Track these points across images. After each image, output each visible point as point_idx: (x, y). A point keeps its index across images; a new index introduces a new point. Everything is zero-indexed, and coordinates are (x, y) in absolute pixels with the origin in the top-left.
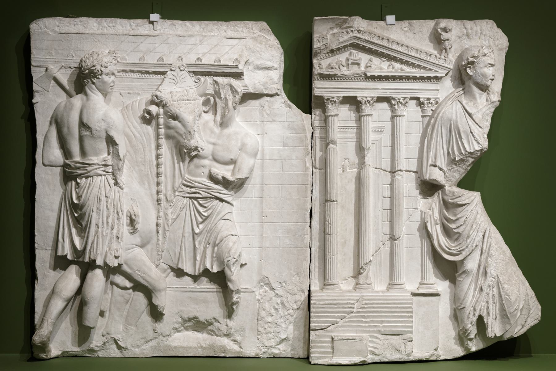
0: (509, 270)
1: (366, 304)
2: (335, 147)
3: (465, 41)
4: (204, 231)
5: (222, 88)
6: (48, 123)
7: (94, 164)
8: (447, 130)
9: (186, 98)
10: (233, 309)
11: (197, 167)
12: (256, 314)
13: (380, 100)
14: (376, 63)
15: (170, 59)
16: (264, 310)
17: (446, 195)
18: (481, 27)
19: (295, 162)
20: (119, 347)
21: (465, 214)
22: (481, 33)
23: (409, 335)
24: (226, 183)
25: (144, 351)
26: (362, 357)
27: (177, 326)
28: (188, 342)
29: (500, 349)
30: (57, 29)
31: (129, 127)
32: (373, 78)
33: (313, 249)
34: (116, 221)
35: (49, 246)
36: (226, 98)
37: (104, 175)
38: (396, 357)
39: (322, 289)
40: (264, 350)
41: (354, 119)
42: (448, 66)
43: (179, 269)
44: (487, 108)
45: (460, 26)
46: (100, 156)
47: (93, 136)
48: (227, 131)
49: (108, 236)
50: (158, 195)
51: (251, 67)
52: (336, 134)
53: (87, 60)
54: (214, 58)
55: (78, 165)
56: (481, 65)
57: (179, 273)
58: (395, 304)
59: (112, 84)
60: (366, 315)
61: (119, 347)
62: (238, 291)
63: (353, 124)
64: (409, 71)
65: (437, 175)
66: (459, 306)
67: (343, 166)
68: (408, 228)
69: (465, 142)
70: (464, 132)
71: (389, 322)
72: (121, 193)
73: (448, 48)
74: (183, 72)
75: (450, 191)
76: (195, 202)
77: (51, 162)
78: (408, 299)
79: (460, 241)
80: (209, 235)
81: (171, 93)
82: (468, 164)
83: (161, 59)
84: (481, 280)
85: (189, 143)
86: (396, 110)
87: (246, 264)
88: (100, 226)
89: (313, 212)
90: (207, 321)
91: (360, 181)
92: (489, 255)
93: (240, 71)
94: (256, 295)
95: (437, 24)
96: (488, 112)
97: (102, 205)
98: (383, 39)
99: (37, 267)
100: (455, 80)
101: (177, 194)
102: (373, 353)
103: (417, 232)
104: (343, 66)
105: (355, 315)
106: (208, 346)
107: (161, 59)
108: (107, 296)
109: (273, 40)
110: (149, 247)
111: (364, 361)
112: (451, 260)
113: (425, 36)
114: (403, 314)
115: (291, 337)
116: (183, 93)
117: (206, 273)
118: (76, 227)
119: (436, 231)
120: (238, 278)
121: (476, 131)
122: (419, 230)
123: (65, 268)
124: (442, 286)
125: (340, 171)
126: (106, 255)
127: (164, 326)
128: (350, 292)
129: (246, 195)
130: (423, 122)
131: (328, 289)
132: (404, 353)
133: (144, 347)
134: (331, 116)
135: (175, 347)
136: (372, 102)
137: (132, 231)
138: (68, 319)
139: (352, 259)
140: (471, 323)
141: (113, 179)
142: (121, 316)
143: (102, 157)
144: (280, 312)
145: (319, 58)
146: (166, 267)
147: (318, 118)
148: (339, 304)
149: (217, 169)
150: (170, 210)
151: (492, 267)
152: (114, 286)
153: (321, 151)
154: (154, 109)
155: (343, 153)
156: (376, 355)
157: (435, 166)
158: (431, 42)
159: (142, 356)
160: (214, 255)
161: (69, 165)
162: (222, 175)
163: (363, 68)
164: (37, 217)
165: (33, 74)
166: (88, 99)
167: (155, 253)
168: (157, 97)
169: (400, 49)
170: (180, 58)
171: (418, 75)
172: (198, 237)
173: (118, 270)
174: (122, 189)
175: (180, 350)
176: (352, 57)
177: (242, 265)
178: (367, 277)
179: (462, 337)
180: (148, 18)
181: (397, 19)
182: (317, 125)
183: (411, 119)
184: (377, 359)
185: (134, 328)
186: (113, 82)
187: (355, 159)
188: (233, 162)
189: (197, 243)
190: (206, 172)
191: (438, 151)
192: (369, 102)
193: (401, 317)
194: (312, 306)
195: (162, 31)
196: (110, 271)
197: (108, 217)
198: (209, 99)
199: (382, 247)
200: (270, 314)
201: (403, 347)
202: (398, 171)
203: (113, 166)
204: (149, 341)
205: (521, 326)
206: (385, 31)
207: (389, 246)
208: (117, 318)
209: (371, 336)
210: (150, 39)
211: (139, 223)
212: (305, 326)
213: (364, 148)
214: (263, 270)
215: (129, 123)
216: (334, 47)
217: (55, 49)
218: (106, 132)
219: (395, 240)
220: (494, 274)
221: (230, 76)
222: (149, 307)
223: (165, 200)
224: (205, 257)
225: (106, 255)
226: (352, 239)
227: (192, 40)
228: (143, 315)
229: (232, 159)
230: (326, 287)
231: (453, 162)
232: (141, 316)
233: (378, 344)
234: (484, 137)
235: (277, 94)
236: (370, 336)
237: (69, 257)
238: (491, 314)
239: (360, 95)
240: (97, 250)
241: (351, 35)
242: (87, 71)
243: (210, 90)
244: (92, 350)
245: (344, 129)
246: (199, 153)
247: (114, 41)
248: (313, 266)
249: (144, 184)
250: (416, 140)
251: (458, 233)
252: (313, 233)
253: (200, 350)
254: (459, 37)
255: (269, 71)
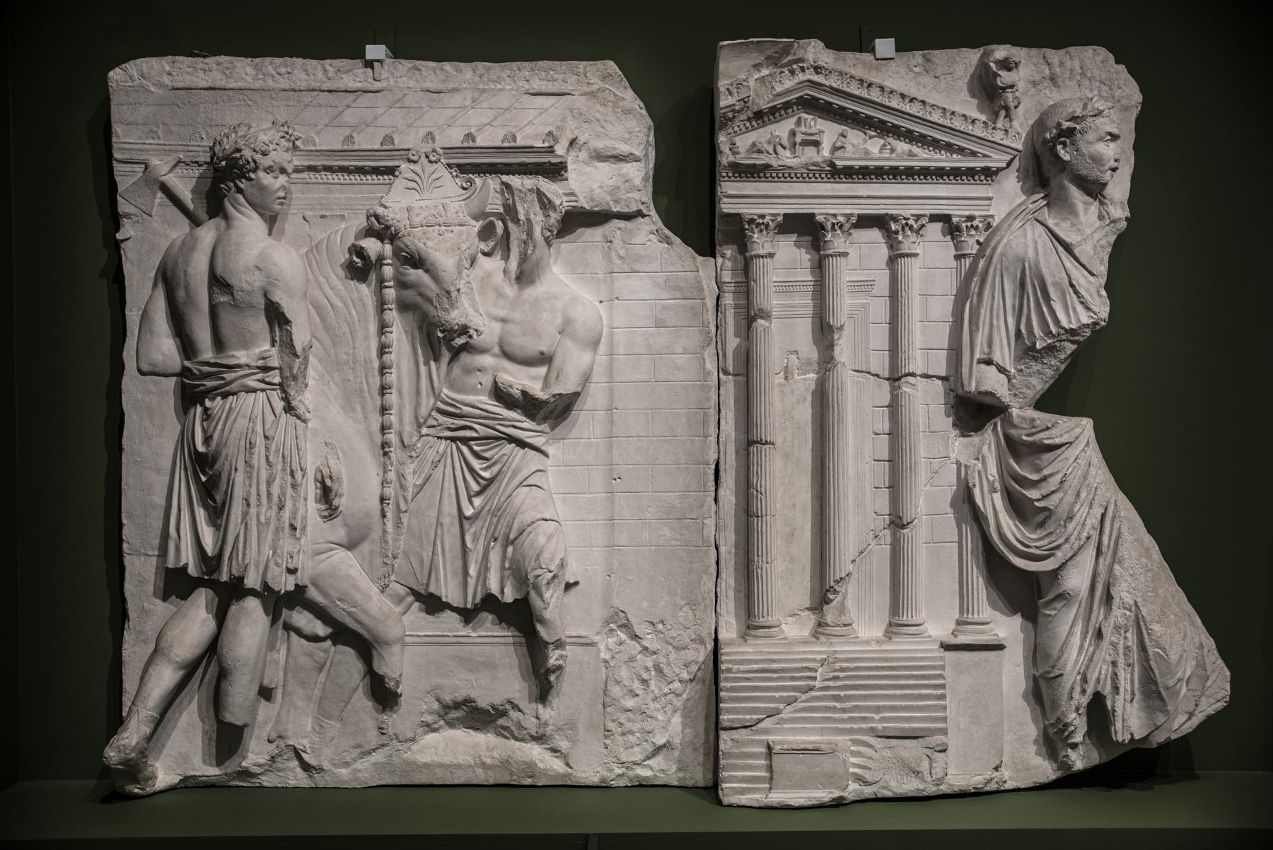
0: (1160, 592)
1: (842, 670)
2: (767, 324)
3: (1047, 91)
4: (484, 513)
5: (521, 198)
6: (150, 284)
7: (239, 366)
8: (1014, 282)
9: (441, 220)
10: (549, 682)
11: (468, 371)
12: (601, 693)
13: (865, 222)
14: (855, 142)
15: (410, 139)
16: (618, 682)
17: (1015, 426)
18: (1082, 61)
19: (681, 360)
20: (306, 767)
21: (1056, 466)
22: (1083, 74)
23: (939, 739)
24: (529, 405)
25: (359, 775)
26: (837, 788)
27: (429, 718)
28: (454, 752)
29: (1132, 767)
30: (166, 80)
31: (321, 288)
32: (850, 173)
33: (722, 549)
34: (289, 491)
35: (152, 549)
36: (529, 220)
37: (263, 390)
38: (910, 786)
39: (744, 636)
40: (618, 771)
41: (809, 264)
42: (1013, 145)
43: (431, 595)
44: (1103, 233)
45: (1035, 60)
46: (256, 348)
47: (235, 305)
48: (530, 292)
49: (272, 526)
50: (384, 434)
51: (583, 155)
52: (769, 296)
53: (225, 140)
54: (502, 133)
55: (207, 369)
56: (1091, 136)
57: (433, 604)
58: (906, 668)
59: (282, 194)
60: (842, 694)
61: (306, 767)
62: (559, 644)
63: (806, 275)
64: (925, 157)
65: (993, 382)
66: (1049, 672)
67: (786, 367)
68: (930, 499)
69: (1057, 306)
70: (1056, 284)
71: (893, 709)
72: (300, 432)
73: (1012, 105)
74: (435, 166)
75: (1024, 418)
76: (465, 449)
77: (153, 365)
78: (936, 658)
79: (1051, 526)
80: (495, 520)
81: (409, 209)
82: (1062, 357)
83: (388, 139)
84: (1098, 614)
85: (448, 318)
86: (900, 242)
87: (576, 583)
88: (253, 501)
89: (722, 468)
90: (493, 707)
91: (823, 400)
92: (1115, 559)
93: (558, 160)
94: (599, 651)
95: (986, 55)
96: (1103, 242)
97: (255, 456)
98: (870, 85)
99: (127, 594)
100: (1027, 177)
101: (425, 430)
102: (858, 778)
103: (950, 510)
104: (784, 148)
105: (818, 693)
106: (496, 762)
107: (388, 139)
108: (275, 655)
109: (629, 97)
110: (365, 548)
111: (842, 798)
112: (1030, 569)
113: (960, 83)
114: (924, 692)
115: (677, 741)
116: (434, 209)
117: (490, 603)
118: (205, 506)
119: (993, 505)
120: (561, 615)
121: (1082, 281)
122: (954, 504)
123: (184, 597)
124: (1007, 628)
125: (779, 379)
126: (266, 567)
127: (399, 721)
128: (805, 643)
129: (575, 432)
130: (959, 269)
131: (757, 636)
132: (929, 778)
133: (359, 765)
134: (759, 256)
135: (426, 765)
136: (847, 226)
137: (326, 513)
138: (194, 706)
139: (808, 570)
140: (1077, 710)
141: (283, 399)
142: (309, 698)
143: (257, 351)
144: (653, 687)
145: (730, 130)
146: (402, 591)
147: (729, 264)
148: (783, 670)
149: (510, 374)
150: (410, 468)
151: (1124, 584)
152: (292, 633)
153: (736, 335)
154: (372, 246)
155: (785, 338)
156: (866, 783)
157: (989, 362)
158: (973, 95)
159: (354, 785)
160: (507, 565)
161: (189, 370)
162: (520, 387)
163: (826, 153)
164: (127, 485)
165: (118, 179)
166: (228, 226)
167: (378, 561)
168: (377, 217)
169: (907, 108)
170: (430, 136)
171: (947, 165)
172: (471, 524)
173: (297, 598)
174: (304, 421)
175: (437, 771)
176: (803, 129)
177: (569, 586)
178: (842, 609)
179: (1053, 740)
180: (360, 55)
181: (899, 49)
182: (728, 280)
183: (932, 265)
184: (868, 791)
185: (338, 725)
186: (284, 188)
187: (809, 351)
188: (544, 359)
189: (468, 538)
190: (487, 381)
191: (995, 330)
192: (841, 227)
193: (921, 697)
194: (722, 676)
195: (392, 81)
196: (278, 603)
197: (269, 483)
198: (492, 224)
199: (873, 543)
200: (631, 691)
201: (925, 764)
202: (907, 375)
203: (281, 369)
204: (369, 753)
205: (1186, 716)
206: (874, 73)
207: (889, 540)
208: (300, 703)
209: (855, 742)
210: (365, 100)
211: (341, 496)
212: (706, 717)
213: (830, 328)
214: (614, 595)
215: (322, 279)
216: (764, 104)
217: (164, 124)
218: (265, 296)
219: (903, 527)
220: (1129, 600)
221: (537, 173)
222: (368, 679)
223: (399, 444)
224: (487, 569)
225: (266, 567)
226: (809, 526)
227: (457, 99)
228: (355, 696)
229: (542, 353)
230: (752, 632)
231: (1027, 352)
232: (350, 698)
233: (870, 758)
234: (1100, 296)
235: (640, 214)
236: (852, 741)
237: (192, 571)
238: (1122, 690)
239: (820, 211)
240: (244, 554)
241: (801, 77)
242: (224, 163)
243: (495, 204)
244: (246, 774)
245: (787, 287)
246: (471, 341)
247: (290, 103)
248: (723, 586)
249: (353, 410)
250: (942, 308)
251: (1045, 509)
252: (722, 513)
253: (480, 771)
254: (1034, 84)
255: (623, 164)
